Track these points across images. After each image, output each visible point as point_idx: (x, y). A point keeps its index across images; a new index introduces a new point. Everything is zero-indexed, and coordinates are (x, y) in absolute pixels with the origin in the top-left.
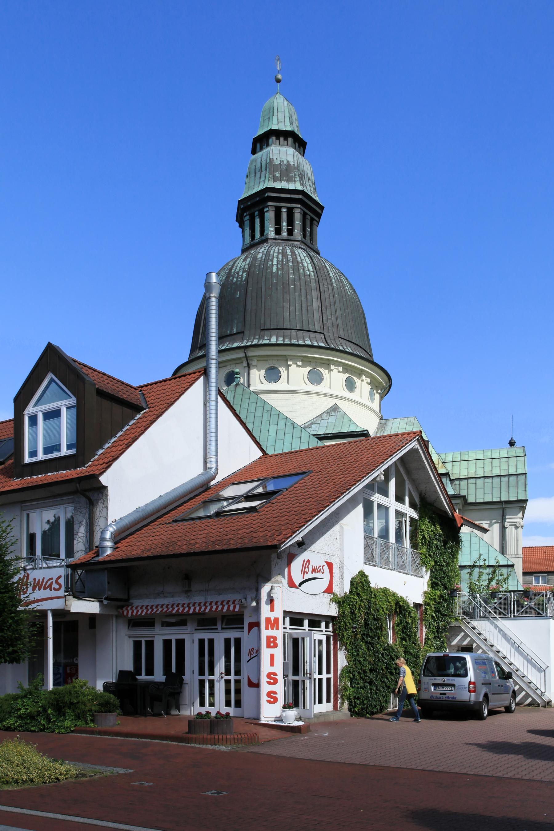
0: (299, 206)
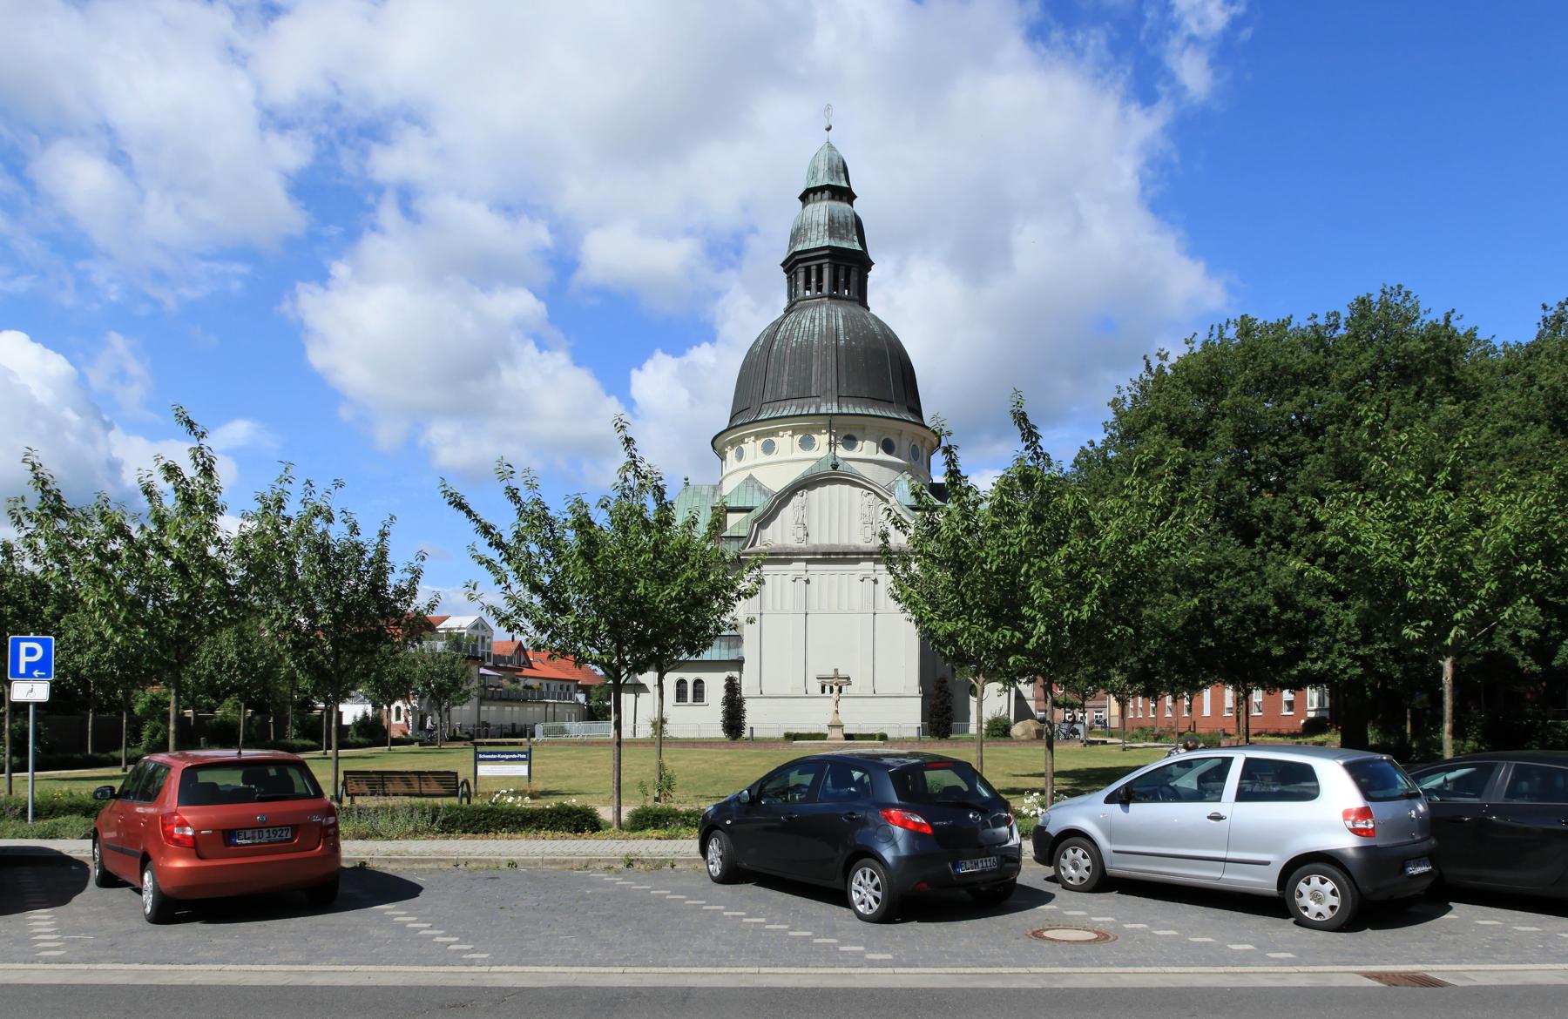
0: (827, 260)
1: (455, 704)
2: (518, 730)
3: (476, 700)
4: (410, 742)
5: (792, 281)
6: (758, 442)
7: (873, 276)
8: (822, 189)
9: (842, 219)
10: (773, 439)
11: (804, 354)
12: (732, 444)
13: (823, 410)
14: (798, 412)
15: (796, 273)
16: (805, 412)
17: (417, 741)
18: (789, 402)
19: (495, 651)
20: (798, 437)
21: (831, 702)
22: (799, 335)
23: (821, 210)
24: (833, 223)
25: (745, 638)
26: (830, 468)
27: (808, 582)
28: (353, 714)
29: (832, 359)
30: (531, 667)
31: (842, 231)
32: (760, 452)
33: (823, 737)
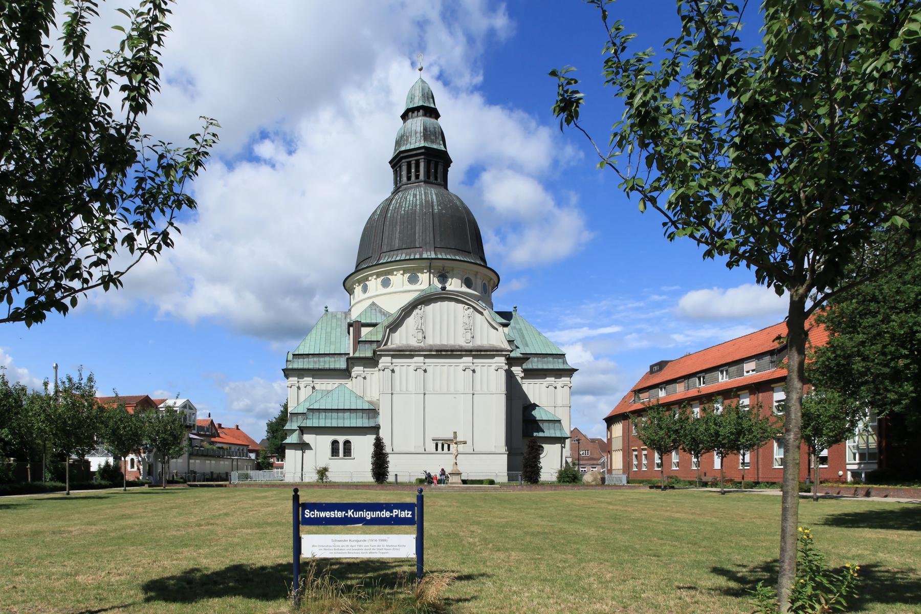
0: (423, 157)
1: (173, 458)
2: (215, 476)
3: (186, 455)
4: (142, 484)
5: (397, 174)
8: (417, 109)
9: (432, 129)
10: (389, 277)
11: (410, 218)
13: (425, 256)
14: (408, 257)
15: (400, 167)
16: (412, 257)
17: (147, 483)
18: (400, 252)
19: (197, 424)
21: (453, 457)
22: (406, 206)
23: (418, 123)
24: (426, 131)
27: (425, 371)
28: (98, 463)
29: (429, 222)
30: (219, 436)
31: (433, 138)
32: (380, 286)
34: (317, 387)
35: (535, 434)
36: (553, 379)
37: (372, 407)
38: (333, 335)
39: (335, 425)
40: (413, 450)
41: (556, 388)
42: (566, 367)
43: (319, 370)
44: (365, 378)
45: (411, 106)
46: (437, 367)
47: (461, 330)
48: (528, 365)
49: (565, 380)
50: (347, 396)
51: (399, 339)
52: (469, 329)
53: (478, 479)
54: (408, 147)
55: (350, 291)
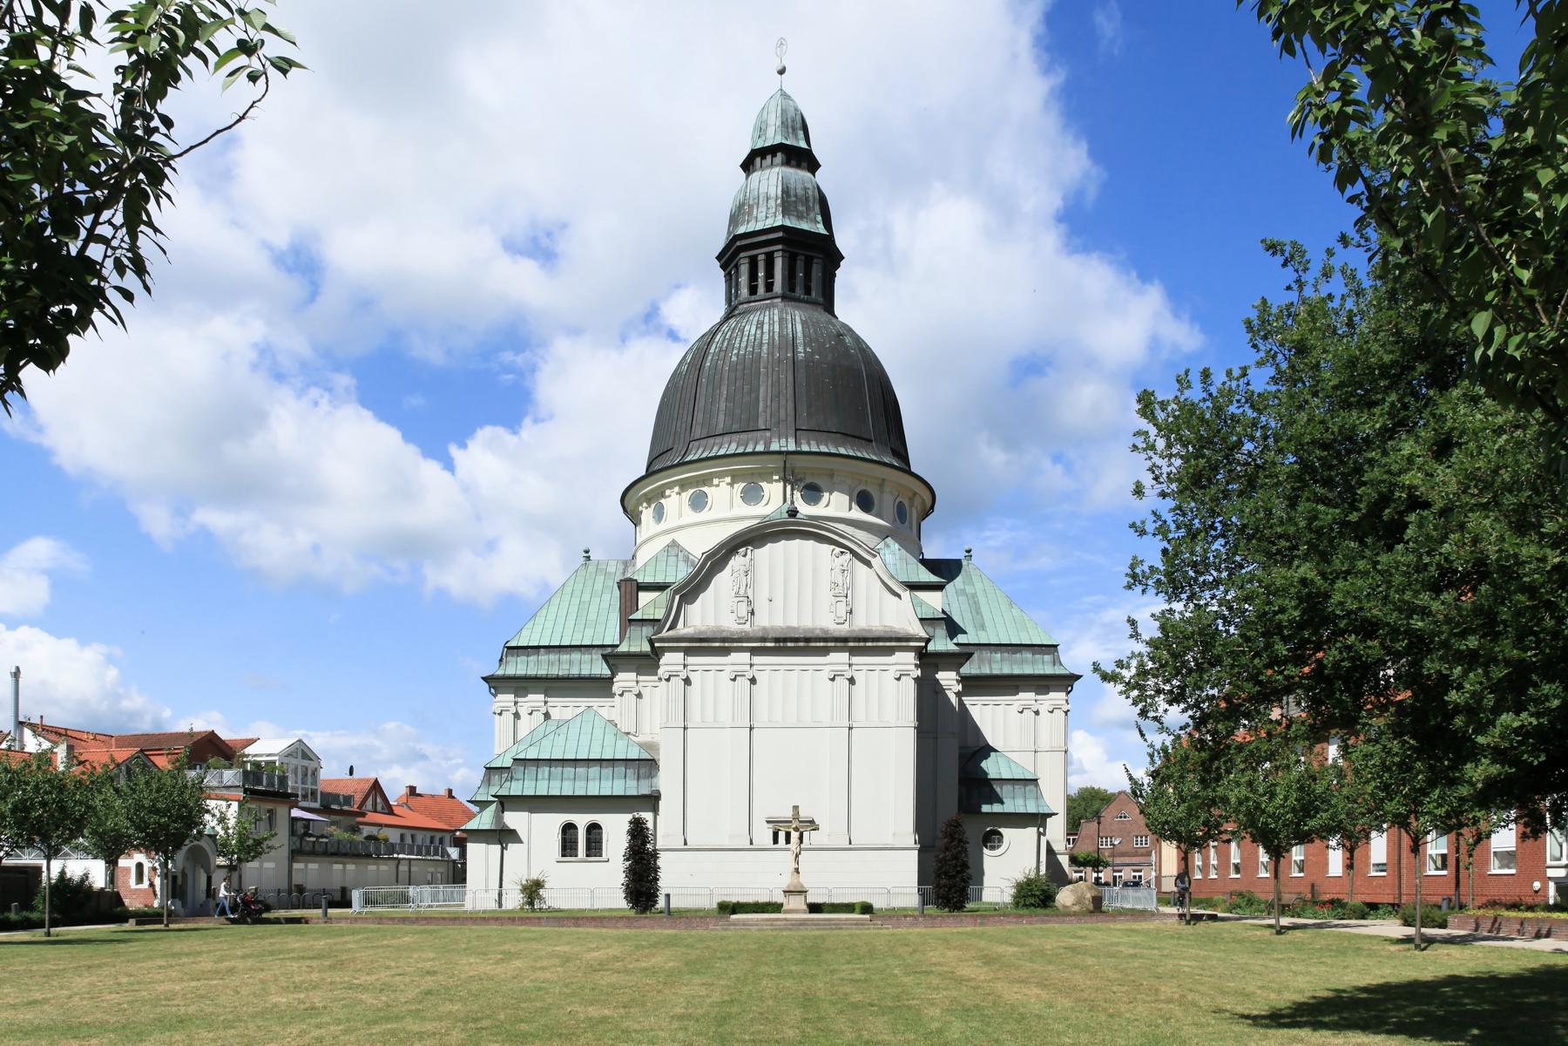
0: (780, 247)
5: (732, 281)
6: (684, 494)
7: (843, 277)
8: (772, 150)
9: (800, 192)
10: (705, 489)
11: (748, 369)
12: (649, 499)
13: (775, 447)
14: (740, 450)
15: (737, 267)
16: (749, 449)
18: (727, 438)
19: (320, 788)
20: (740, 486)
22: (741, 345)
23: (771, 179)
25: (661, 764)
26: (786, 515)
27: (753, 681)
29: (786, 378)
31: (801, 208)
33: (776, 907)
34: (555, 714)
35: (986, 808)
36: (1032, 695)
37: (645, 756)
38: (593, 608)
39: (567, 792)
40: (727, 844)
41: (1037, 713)
42: (1058, 671)
43: (558, 679)
44: (639, 696)
45: (760, 145)
46: (778, 672)
47: (826, 597)
48: (969, 669)
49: (1057, 697)
50: (598, 733)
51: (702, 616)
52: (845, 594)
53: (846, 901)
54: (751, 227)
55: (635, 519)
